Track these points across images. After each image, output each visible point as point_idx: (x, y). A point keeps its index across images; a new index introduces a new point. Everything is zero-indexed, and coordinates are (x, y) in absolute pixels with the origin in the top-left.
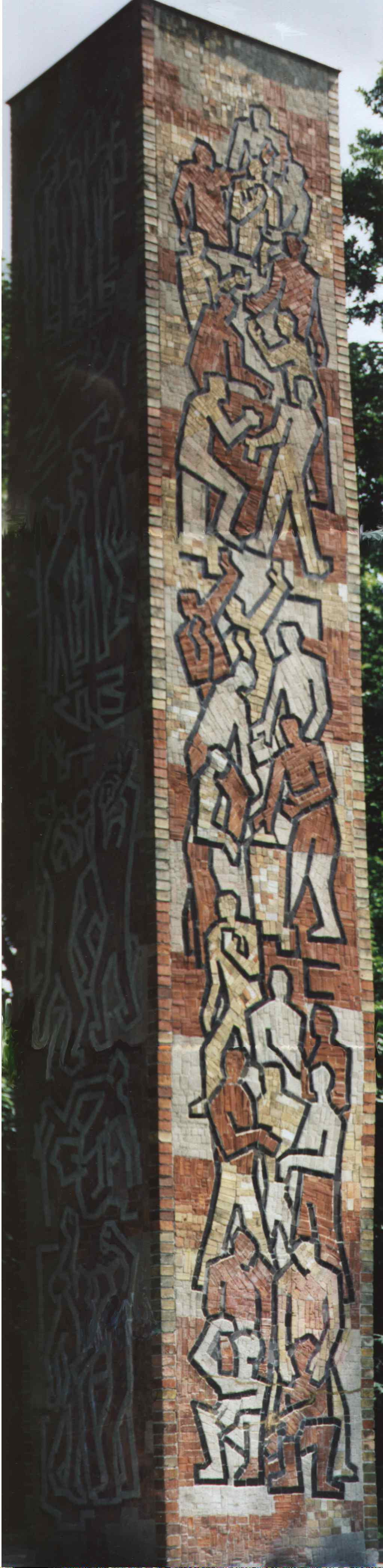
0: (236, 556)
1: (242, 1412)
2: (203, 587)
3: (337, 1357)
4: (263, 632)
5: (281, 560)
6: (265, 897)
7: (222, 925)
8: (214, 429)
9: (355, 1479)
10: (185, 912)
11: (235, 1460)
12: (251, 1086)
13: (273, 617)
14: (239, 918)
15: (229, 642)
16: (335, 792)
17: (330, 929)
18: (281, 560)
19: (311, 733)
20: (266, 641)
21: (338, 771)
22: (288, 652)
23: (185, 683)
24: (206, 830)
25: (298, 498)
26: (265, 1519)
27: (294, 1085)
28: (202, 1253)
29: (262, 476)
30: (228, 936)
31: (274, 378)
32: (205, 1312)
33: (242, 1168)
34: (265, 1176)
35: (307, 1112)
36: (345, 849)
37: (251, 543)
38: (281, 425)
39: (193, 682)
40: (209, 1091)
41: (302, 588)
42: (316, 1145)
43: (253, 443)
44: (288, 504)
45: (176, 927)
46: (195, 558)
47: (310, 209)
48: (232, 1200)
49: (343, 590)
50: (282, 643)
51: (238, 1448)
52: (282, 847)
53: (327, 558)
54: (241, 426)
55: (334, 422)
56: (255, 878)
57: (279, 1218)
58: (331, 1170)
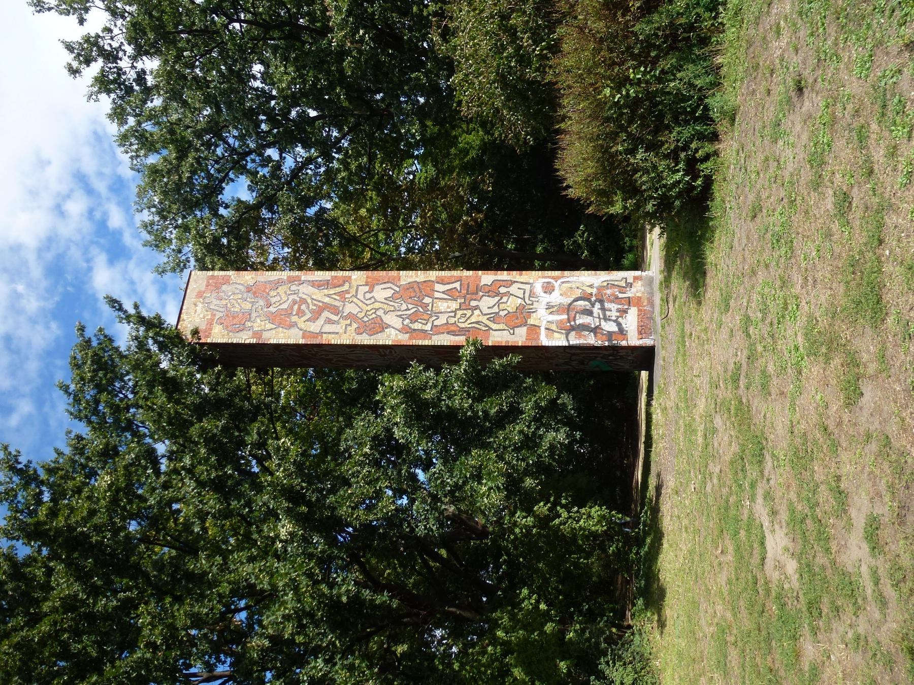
0: (345, 314)
4: (367, 305)
5: (345, 299)
6: (448, 307)
8: (307, 320)
10: (453, 335)
13: (362, 301)
14: (455, 317)
15: (371, 317)
18: (345, 299)
19: (398, 289)
20: (239, 284)
21: (410, 280)
24: (428, 327)
25: (326, 292)
27: (505, 299)
29: (321, 304)
31: (291, 297)
33: (529, 317)
35: (512, 295)
36: (433, 279)
37: (341, 309)
38: (305, 297)
39: (382, 330)
41: (353, 292)
43: (311, 307)
44: (328, 296)
45: (457, 338)
46: (346, 328)
47: (236, 283)
49: (354, 277)
50: (370, 299)
53: (344, 282)
54: (307, 311)
55: (303, 278)
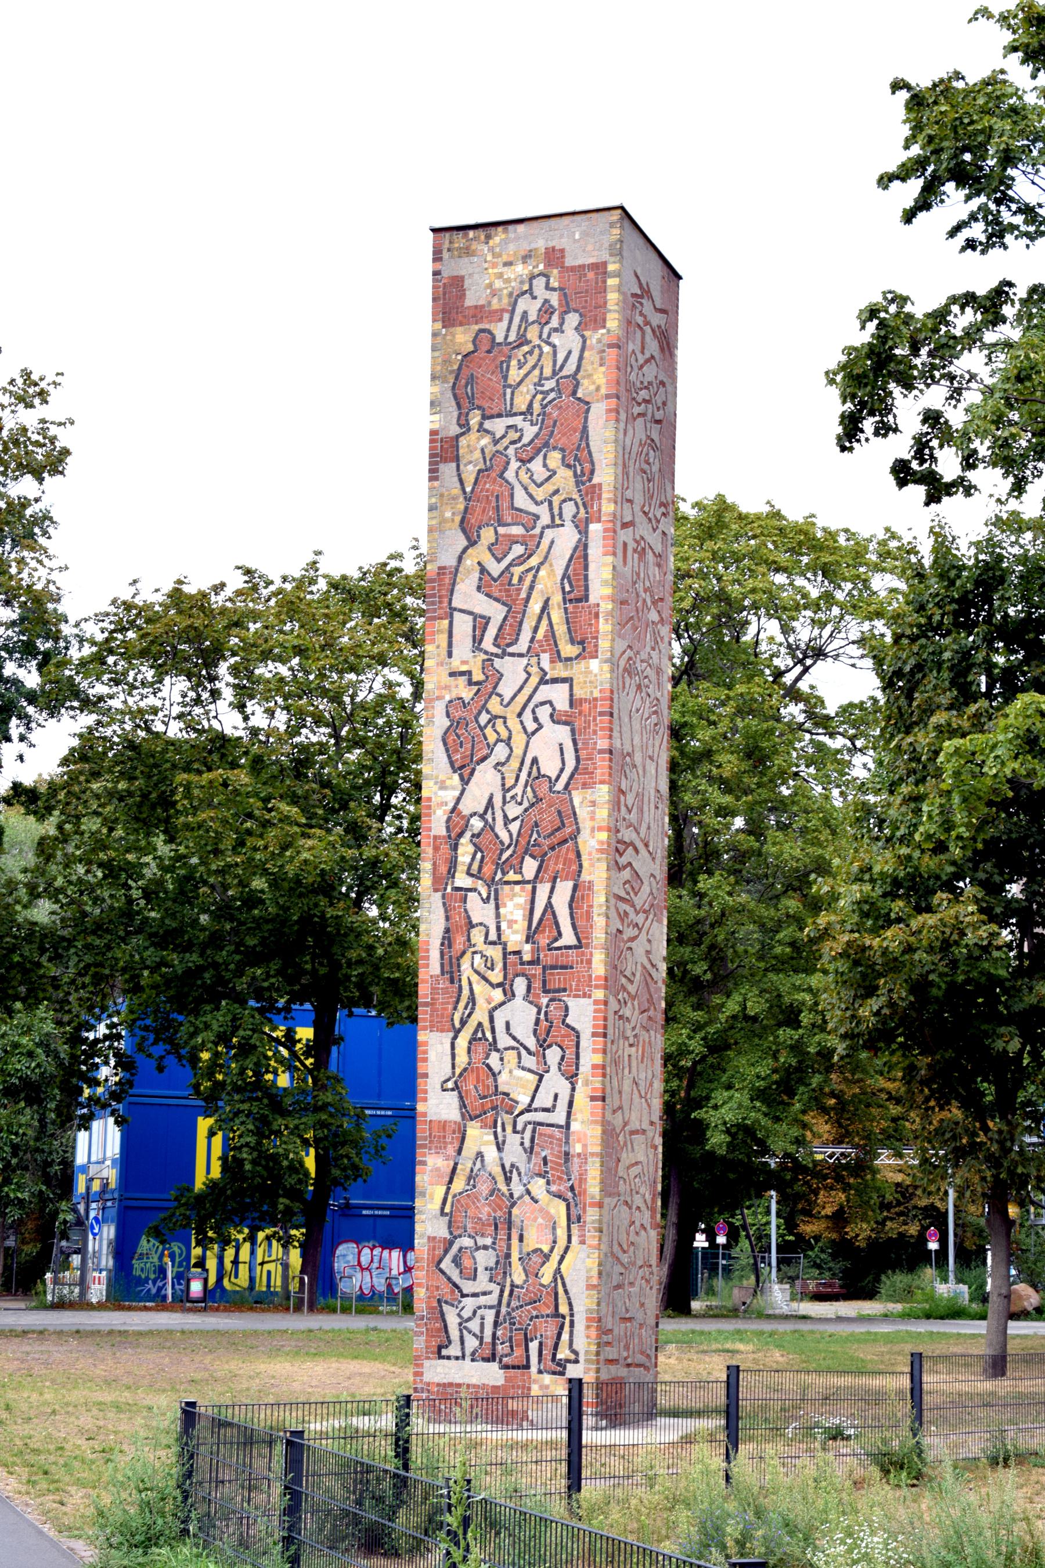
1: (480, 1308)
2: (467, 694)
3: (563, 1267)
7: (472, 950)
9: (576, 1361)
11: (471, 1343)
12: (493, 1066)
16: (578, 830)
17: (568, 938)
22: (540, 727)
23: (450, 770)
24: (462, 880)
25: (557, 598)
26: (498, 1387)
28: (449, 1189)
29: (523, 595)
30: (477, 957)
32: (451, 1233)
34: (504, 1130)
40: (458, 1071)
42: (549, 1104)
46: (462, 674)
48: (475, 1150)
49: (594, 664)
51: (474, 1335)
52: (528, 882)
56: (502, 911)
57: (515, 1160)
58: (563, 1122)
